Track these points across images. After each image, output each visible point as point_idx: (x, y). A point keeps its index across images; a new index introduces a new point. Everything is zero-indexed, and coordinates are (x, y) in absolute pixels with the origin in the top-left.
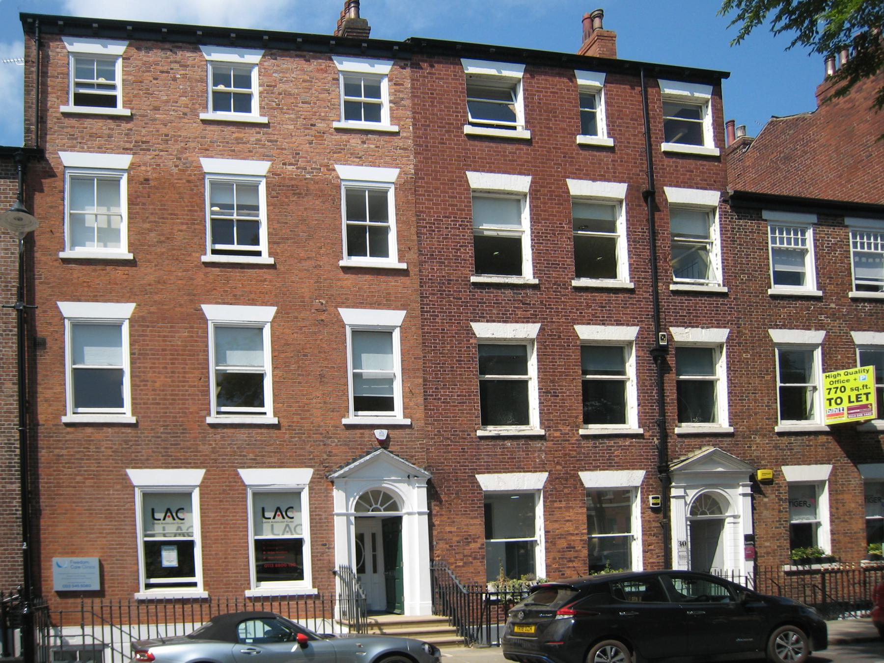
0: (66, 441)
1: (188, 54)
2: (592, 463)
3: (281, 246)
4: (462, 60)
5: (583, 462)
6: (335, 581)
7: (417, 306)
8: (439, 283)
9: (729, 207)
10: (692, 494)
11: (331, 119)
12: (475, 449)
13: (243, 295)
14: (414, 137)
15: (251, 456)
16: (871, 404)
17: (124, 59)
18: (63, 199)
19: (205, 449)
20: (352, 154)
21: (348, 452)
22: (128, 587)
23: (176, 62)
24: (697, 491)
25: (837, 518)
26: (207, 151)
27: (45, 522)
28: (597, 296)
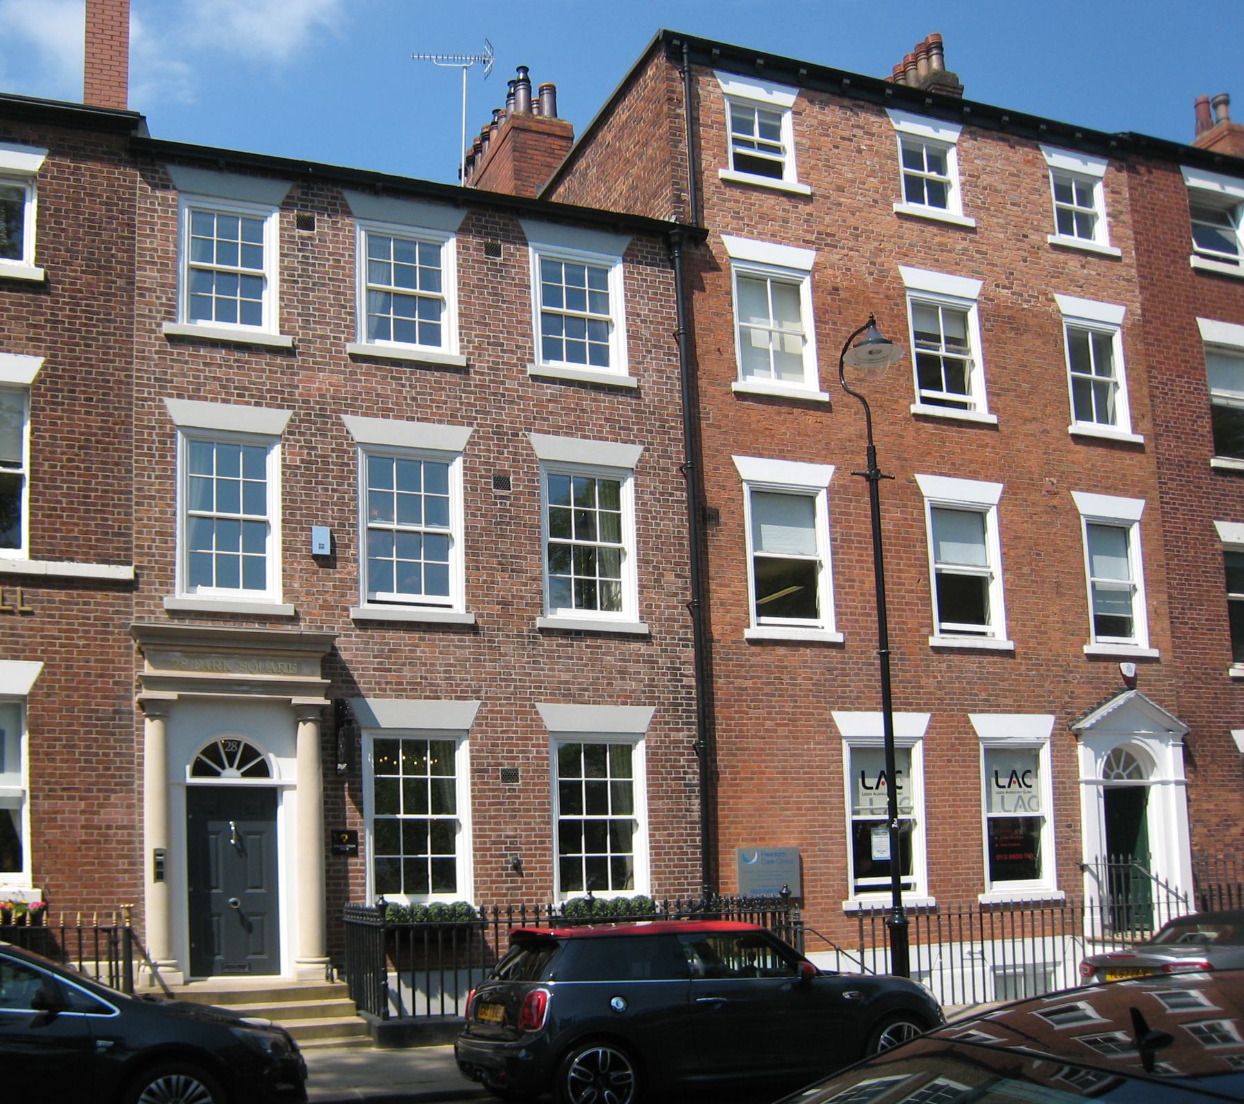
0: (751, 666)
1: (873, 119)
3: (1002, 398)
4: (1183, 168)
6: (1082, 881)
7: (1156, 494)
8: (1177, 465)
11: (1045, 230)
13: (962, 465)
14: (1138, 265)
15: (983, 695)
17: (794, 113)
18: (731, 305)
19: (929, 683)
20: (1071, 281)
21: (1091, 693)
22: (834, 891)
23: (858, 127)
26: (906, 256)
27: (724, 791)
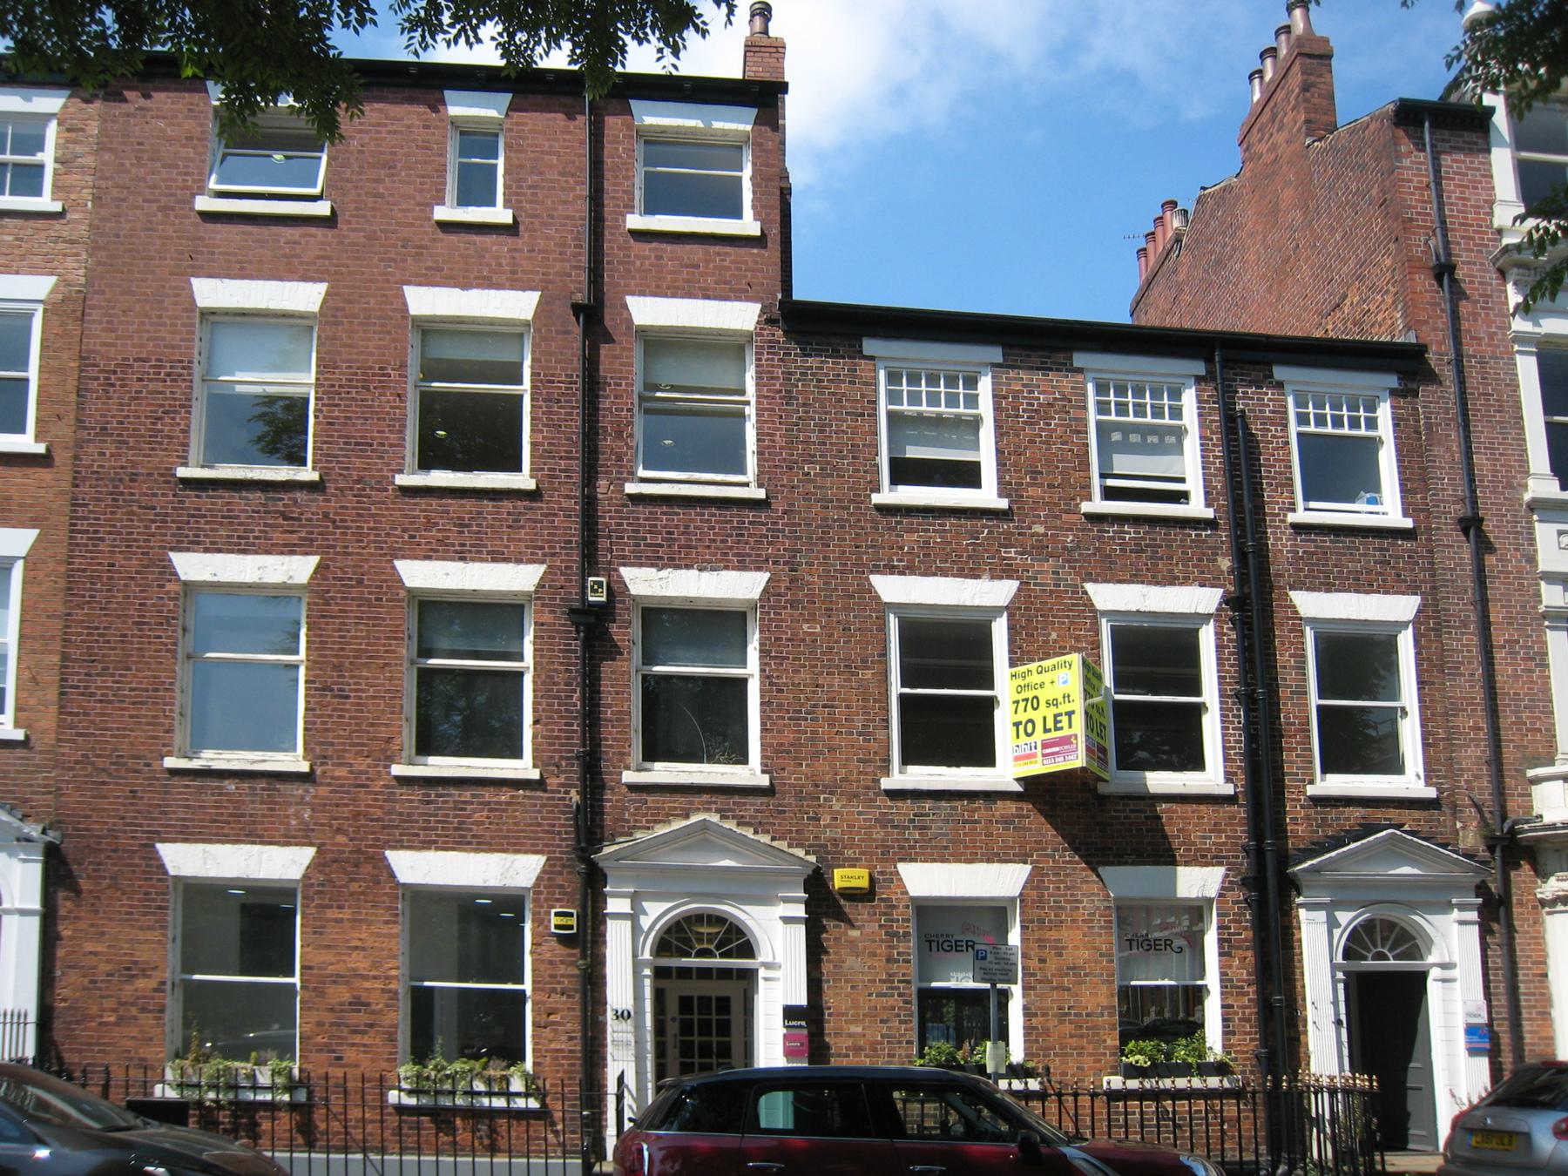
2: (418, 835)
5: (397, 832)
9: (781, 332)
10: (656, 913)
12: (159, 793)
16: (1076, 736)
24: (669, 905)
25: (1041, 982)
28: (451, 505)
